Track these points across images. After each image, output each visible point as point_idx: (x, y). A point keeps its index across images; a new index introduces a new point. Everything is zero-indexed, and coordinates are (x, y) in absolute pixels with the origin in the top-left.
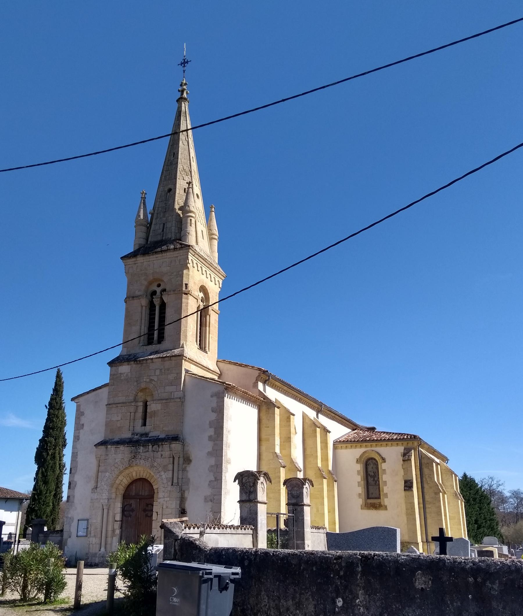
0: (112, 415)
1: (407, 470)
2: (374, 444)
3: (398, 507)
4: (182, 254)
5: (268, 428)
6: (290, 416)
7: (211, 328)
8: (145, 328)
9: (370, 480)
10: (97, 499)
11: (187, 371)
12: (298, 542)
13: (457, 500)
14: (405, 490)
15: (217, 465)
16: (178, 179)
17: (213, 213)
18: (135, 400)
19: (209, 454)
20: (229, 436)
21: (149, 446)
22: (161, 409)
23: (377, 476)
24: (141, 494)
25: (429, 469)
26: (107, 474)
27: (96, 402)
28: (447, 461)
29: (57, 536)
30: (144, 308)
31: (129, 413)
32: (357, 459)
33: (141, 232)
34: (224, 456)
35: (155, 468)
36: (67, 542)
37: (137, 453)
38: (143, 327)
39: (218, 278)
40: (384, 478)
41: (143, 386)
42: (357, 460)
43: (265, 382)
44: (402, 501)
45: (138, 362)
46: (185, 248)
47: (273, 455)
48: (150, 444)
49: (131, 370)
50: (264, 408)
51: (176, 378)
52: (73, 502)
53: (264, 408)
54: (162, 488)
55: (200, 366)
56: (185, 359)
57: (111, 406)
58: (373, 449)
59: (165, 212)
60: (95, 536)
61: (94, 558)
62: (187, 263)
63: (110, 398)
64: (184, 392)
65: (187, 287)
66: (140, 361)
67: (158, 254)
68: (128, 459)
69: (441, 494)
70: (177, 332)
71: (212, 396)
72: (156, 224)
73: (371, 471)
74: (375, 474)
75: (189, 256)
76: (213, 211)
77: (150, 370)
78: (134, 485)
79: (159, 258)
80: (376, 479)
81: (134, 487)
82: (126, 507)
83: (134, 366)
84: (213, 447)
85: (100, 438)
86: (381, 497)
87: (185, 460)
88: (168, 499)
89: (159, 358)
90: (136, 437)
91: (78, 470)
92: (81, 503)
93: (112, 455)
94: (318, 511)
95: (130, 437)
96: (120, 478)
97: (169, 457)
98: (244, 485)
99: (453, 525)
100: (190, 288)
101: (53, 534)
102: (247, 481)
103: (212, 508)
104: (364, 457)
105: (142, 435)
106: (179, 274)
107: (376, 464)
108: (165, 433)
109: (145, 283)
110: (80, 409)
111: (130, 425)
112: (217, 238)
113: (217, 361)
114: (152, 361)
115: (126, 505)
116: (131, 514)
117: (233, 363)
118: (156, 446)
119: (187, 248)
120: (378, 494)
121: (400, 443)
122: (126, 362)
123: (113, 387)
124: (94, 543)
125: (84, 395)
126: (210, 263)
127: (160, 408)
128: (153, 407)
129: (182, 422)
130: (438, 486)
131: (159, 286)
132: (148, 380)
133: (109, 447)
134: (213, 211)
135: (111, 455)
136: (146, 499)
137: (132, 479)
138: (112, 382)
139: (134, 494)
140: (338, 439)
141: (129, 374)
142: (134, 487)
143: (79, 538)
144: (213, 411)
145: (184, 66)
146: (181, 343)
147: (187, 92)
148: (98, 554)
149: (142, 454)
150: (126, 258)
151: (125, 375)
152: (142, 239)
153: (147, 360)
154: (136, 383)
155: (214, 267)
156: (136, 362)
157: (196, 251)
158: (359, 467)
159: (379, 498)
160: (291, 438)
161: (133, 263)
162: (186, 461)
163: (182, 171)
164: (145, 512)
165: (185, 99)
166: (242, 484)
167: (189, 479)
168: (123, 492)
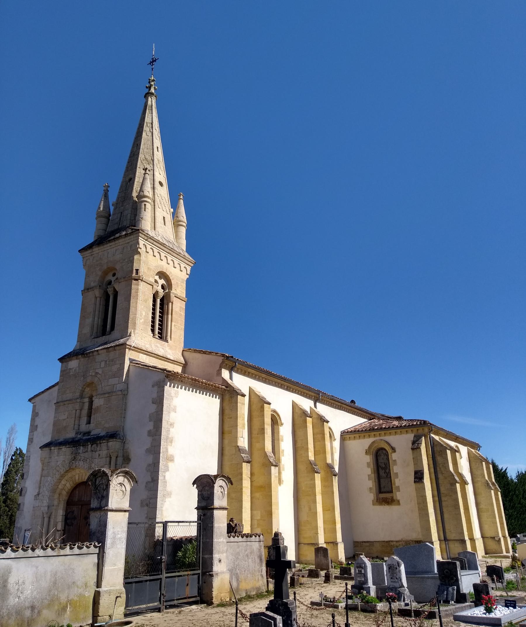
1: (418, 460)
2: (383, 432)
3: (411, 501)
5: (231, 419)
6: (264, 405)
7: (173, 316)
8: (98, 320)
9: (382, 472)
11: (131, 360)
12: (206, 556)
13: (489, 490)
14: (415, 482)
15: (154, 464)
16: (138, 168)
17: (182, 201)
18: (82, 397)
19: (148, 451)
20: (171, 429)
21: (88, 445)
22: (104, 405)
23: (388, 467)
24: (83, 499)
28: (478, 448)
30: (98, 299)
31: (75, 411)
32: (366, 450)
33: (101, 223)
34: (163, 452)
37: (77, 454)
38: (96, 319)
39: (185, 264)
40: (395, 469)
41: (89, 380)
42: (366, 452)
43: (231, 369)
44: (414, 494)
45: (85, 355)
46: (135, 232)
47: (235, 449)
48: (89, 443)
50: (227, 397)
53: (227, 397)
55: (153, 355)
56: (130, 347)
57: (59, 404)
58: (382, 438)
59: (124, 201)
62: (138, 248)
64: (127, 384)
65: (138, 273)
66: (87, 354)
67: (111, 242)
68: (69, 461)
69: (458, 485)
70: (125, 321)
71: (153, 386)
73: (381, 463)
74: (386, 466)
75: (140, 241)
76: (181, 199)
77: (96, 363)
78: (77, 489)
80: (387, 471)
81: (77, 492)
82: (69, 515)
83: (82, 359)
84: (151, 443)
85: (47, 439)
86: (394, 491)
89: (104, 349)
90: (79, 436)
94: (310, 509)
95: (74, 437)
96: (63, 482)
98: (97, 489)
99: (487, 518)
100: (141, 273)
102: (100, 483)
103: (147, 514)
104: (373, 448)
105: (85, 434)
106: (130, 260)
107: (386, 455)
109: (100, 273)
111: (75, 423)
112: (185, 225)
113: (183, 351)
114: (98, 353)
115: (69, 513)
116: (73, 522)
117: (198, 351)
119: (137, 232)
120: (390, 488)
121: (409, 430)
123: (63, 383)
126: (170, 249)
128: (98, 402)
129: (123, 417)
130: (454, 476)
131: (114, 275)
132: (93, 374)
133: (53, 448)
134: (181, 199)
140: (347, 429)
141: (77, 369)
142: (77, 492)
144: (153, 403)
145: (153, 64)
146: (129, 332)
147: (155, 88)
149: (82, 455)
150: (83, 250)
151: (73, 371)
152: (101, 231)
153: (93, 353)
155: (177, 253)
156: (83, 356)
157: (148, 236)
158: (368, 459)
159: (391, 492)
160: (264, 429)
161: (90, 254)
162: (125, 461)
163: (143, 160)
165: (152, 94)
166: (95, 486)
168: (66, 498)
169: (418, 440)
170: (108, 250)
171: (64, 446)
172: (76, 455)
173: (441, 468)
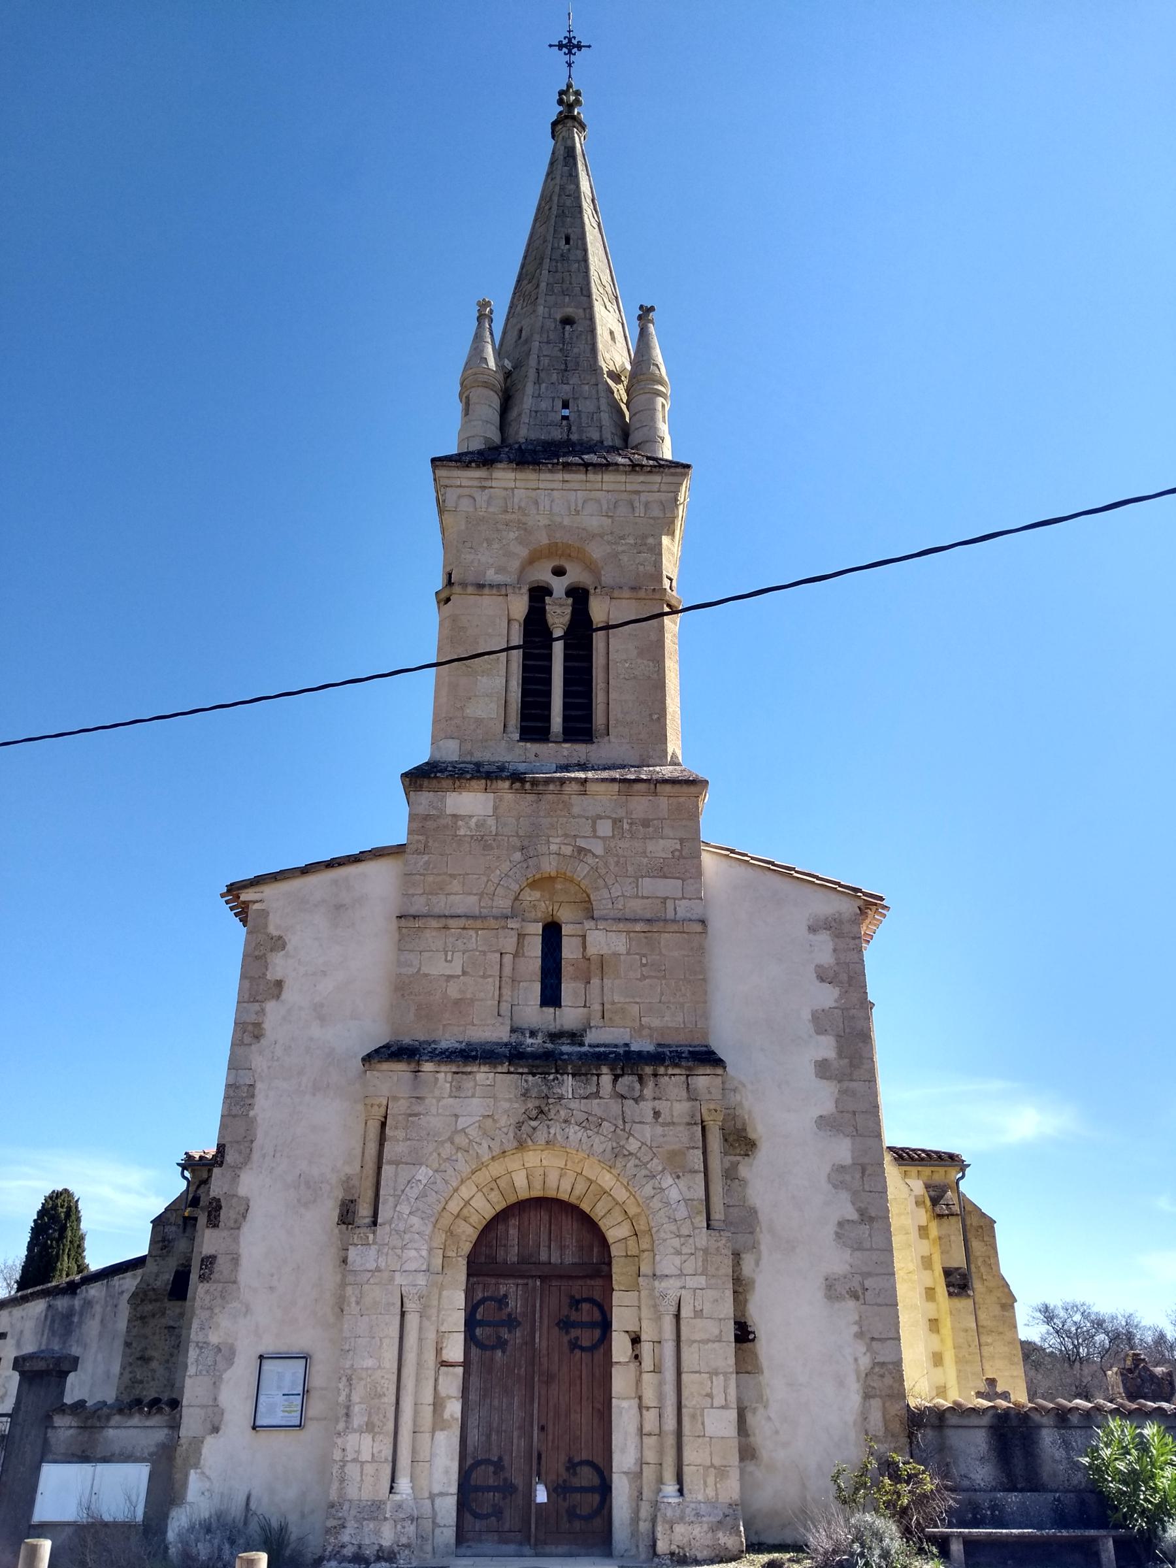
0: (426, 954)
4: (656, 487)
10: (378, 1269)
21: (598, 1075)
22: (628, 953)
24: (544, 1257)
25: (984, 1241)
26: (423, 1174)
27: (339, 907)
29: (148, 1423)
35: (633, 1161)
36: (198, 1452)
37: (551, 1101)
41: (549, 866)
45: (528, 786)
48: (605, 1070)
49: (495, 808)
51: (677, 854)
52: (235, 1282)
54: (670, 1236)
60: (370, 1427)
61: (371, 1526)
63: (413, 895)
67: (571, 472)
68: (512, 1121)
70: (651, 715)
72: (539, 396)
78: (514, 1222)
79: (576, 486)
81: (513, 1232)
82: (481, 1310)
85: (378, 1035)
87: (731, 1139)
88: (702, 1281)
89: (614, 780)
91: (256, 1156)
92: (272, 1289)
93: (439, 1099)
95: (505, 1040)
97: (689, 1124)
101: (131, 1415)
103: (859, 1323)
108: (651, 1036)
109: (524, 552)
110: (266, 926)
111: (500, 995)
115: (483, 1301)
118: (631, 1078)
122: (478, 778)
123: (426, 858)
124: (366, 1456)
125: (285, 878)
127: (622, 949)
132: (567, 850)
133: (428, 1067)
135: (434, 1101)
136: (570, 1277)
137: (512, 1200)
138: (418, 841)
139: (515, 1259)
141: (491, 822)
142: (513, 1232)
143: (263, 1435)
144: (822, 980)
148: (388, 1507)
149: (574, 1105)
150: (454, 464)
154: (518, 856)
156: (517, 785)
161: (476, 483)
164: (567, 1333)
167: (753, 1212)
168: (467, 1247)
169: (942, 1196)
170: (552, 490)
171: (485, 1064)
172: (548, 1104)
173: (979, 1267)
